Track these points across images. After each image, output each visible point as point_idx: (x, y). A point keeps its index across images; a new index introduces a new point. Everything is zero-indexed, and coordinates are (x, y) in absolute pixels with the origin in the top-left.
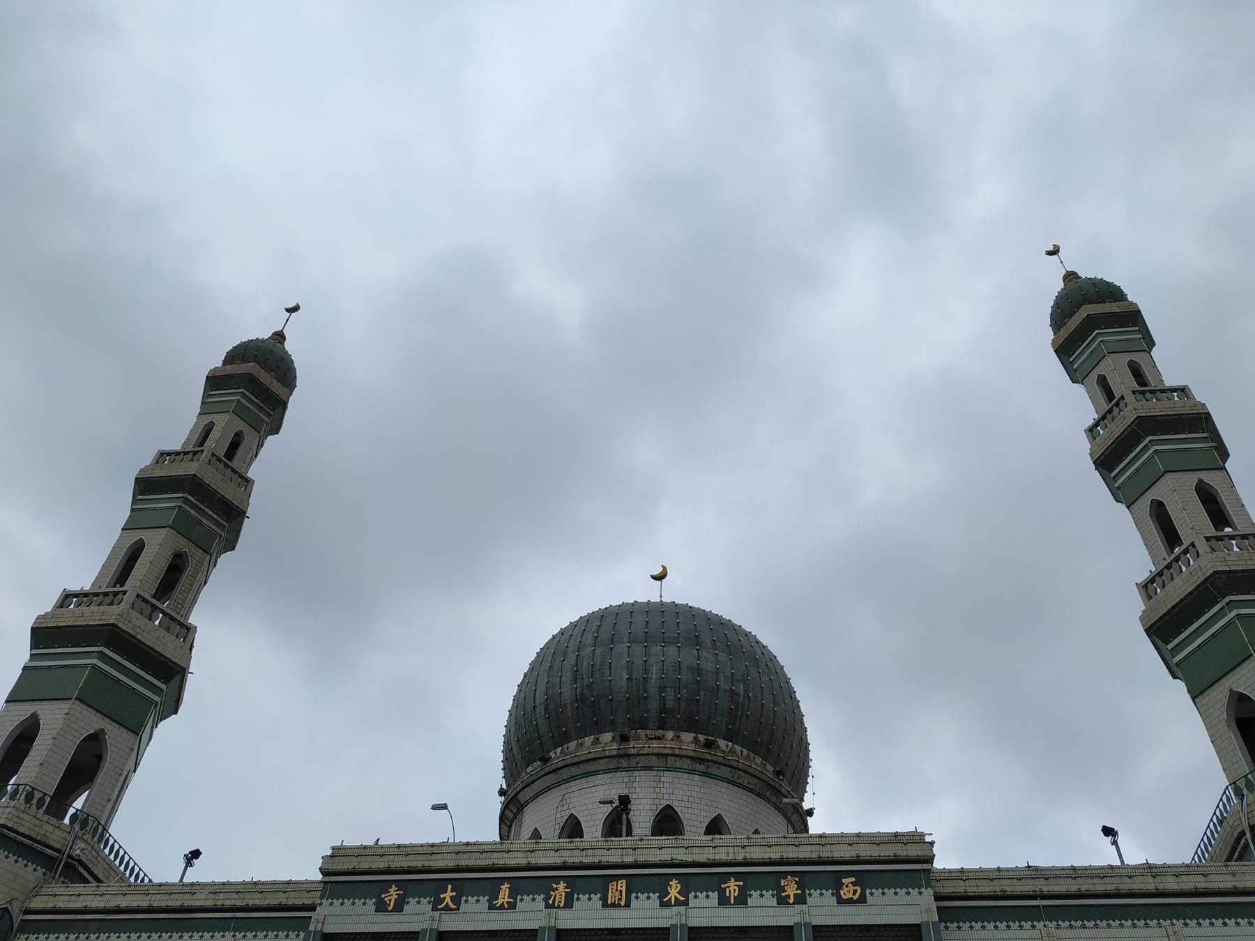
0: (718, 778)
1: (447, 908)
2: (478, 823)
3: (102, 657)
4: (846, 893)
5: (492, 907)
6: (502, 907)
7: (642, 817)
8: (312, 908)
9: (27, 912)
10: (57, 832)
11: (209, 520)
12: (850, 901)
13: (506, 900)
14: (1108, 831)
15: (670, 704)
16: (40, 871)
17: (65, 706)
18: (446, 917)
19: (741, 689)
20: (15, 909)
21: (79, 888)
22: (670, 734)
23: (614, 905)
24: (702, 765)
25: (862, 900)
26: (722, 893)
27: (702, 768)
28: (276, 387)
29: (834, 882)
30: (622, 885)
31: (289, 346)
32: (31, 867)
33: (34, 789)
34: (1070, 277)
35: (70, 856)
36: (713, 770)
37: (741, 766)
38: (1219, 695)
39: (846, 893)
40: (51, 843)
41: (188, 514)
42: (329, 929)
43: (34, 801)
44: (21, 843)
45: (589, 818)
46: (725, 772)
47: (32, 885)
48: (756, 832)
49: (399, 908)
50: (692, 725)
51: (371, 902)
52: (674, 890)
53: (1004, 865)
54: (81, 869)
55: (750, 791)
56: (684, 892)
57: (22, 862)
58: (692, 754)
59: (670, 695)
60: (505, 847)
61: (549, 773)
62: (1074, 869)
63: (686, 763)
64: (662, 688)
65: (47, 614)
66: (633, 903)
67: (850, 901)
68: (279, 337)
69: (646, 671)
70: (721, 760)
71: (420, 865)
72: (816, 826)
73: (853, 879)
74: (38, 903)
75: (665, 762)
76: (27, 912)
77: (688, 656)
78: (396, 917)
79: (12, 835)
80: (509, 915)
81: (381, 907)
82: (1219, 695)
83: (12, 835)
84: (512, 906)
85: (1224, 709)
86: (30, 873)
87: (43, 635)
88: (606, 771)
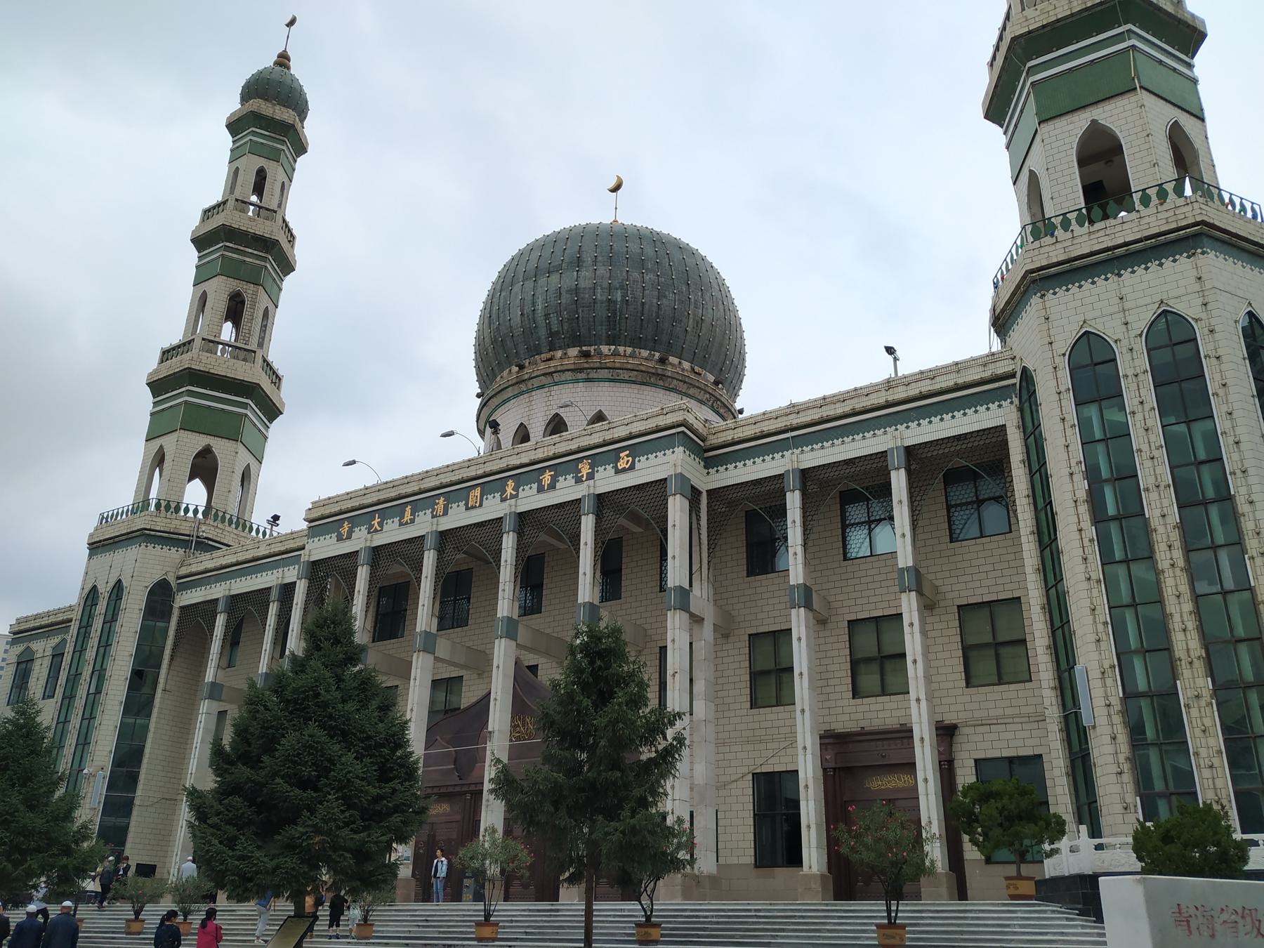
0: (600, 380)
1: (376, 531)
2: (469, 445)
3: (190, 393)
4: (621, 465)
6: (407, 523)
7: (576, 421)
8: (303, 548)
9: (179, 578)
11: (250, 257)
12: (624, 470)
14: (890, 350)
15: (555, 328)
16: (181, 551)
17: (174, 436)
18: (376, 536)
19: (618, 295)
20: (171, 579)
21: (216, 554)
22: (559, 354)
23: (473, 507)
24: (584, 373)
25: (632, 467)
26: (540, 482)
27: (583, 376)
28: (286, 115)
29: (499, 486)
30: (478, 491)
31: (296, 69)
32: (174, 550)
34: (1163, 571)
36: (593, 375)
37: (617, 365)
39: (621, 465)
41: (232, 259)
46: (604, 373)
48: (599, 417)
49: (552, 486)
50: (576, 341)
51: (334, 535)
52: (585, 469)
55: (634, 382)
56: (516, 489)
58: (572, 367)
59: (554, 319)
63: (569, 375)
64: (547, 316)
66: (485, 502)
67: (624, 470)
68: (283, 60)
69: (534, 304)
70: (598, 365)
71: (375, 499)
72: (764, 391)
74: (183, 571)
75: (552, 378)
77: (568, 280)
78: (348, 543)
80: (630, 475)
81: (340, 539)
84: (412, 521)
86: (175, 554)
87: (158, 386)
88: (515, 396)
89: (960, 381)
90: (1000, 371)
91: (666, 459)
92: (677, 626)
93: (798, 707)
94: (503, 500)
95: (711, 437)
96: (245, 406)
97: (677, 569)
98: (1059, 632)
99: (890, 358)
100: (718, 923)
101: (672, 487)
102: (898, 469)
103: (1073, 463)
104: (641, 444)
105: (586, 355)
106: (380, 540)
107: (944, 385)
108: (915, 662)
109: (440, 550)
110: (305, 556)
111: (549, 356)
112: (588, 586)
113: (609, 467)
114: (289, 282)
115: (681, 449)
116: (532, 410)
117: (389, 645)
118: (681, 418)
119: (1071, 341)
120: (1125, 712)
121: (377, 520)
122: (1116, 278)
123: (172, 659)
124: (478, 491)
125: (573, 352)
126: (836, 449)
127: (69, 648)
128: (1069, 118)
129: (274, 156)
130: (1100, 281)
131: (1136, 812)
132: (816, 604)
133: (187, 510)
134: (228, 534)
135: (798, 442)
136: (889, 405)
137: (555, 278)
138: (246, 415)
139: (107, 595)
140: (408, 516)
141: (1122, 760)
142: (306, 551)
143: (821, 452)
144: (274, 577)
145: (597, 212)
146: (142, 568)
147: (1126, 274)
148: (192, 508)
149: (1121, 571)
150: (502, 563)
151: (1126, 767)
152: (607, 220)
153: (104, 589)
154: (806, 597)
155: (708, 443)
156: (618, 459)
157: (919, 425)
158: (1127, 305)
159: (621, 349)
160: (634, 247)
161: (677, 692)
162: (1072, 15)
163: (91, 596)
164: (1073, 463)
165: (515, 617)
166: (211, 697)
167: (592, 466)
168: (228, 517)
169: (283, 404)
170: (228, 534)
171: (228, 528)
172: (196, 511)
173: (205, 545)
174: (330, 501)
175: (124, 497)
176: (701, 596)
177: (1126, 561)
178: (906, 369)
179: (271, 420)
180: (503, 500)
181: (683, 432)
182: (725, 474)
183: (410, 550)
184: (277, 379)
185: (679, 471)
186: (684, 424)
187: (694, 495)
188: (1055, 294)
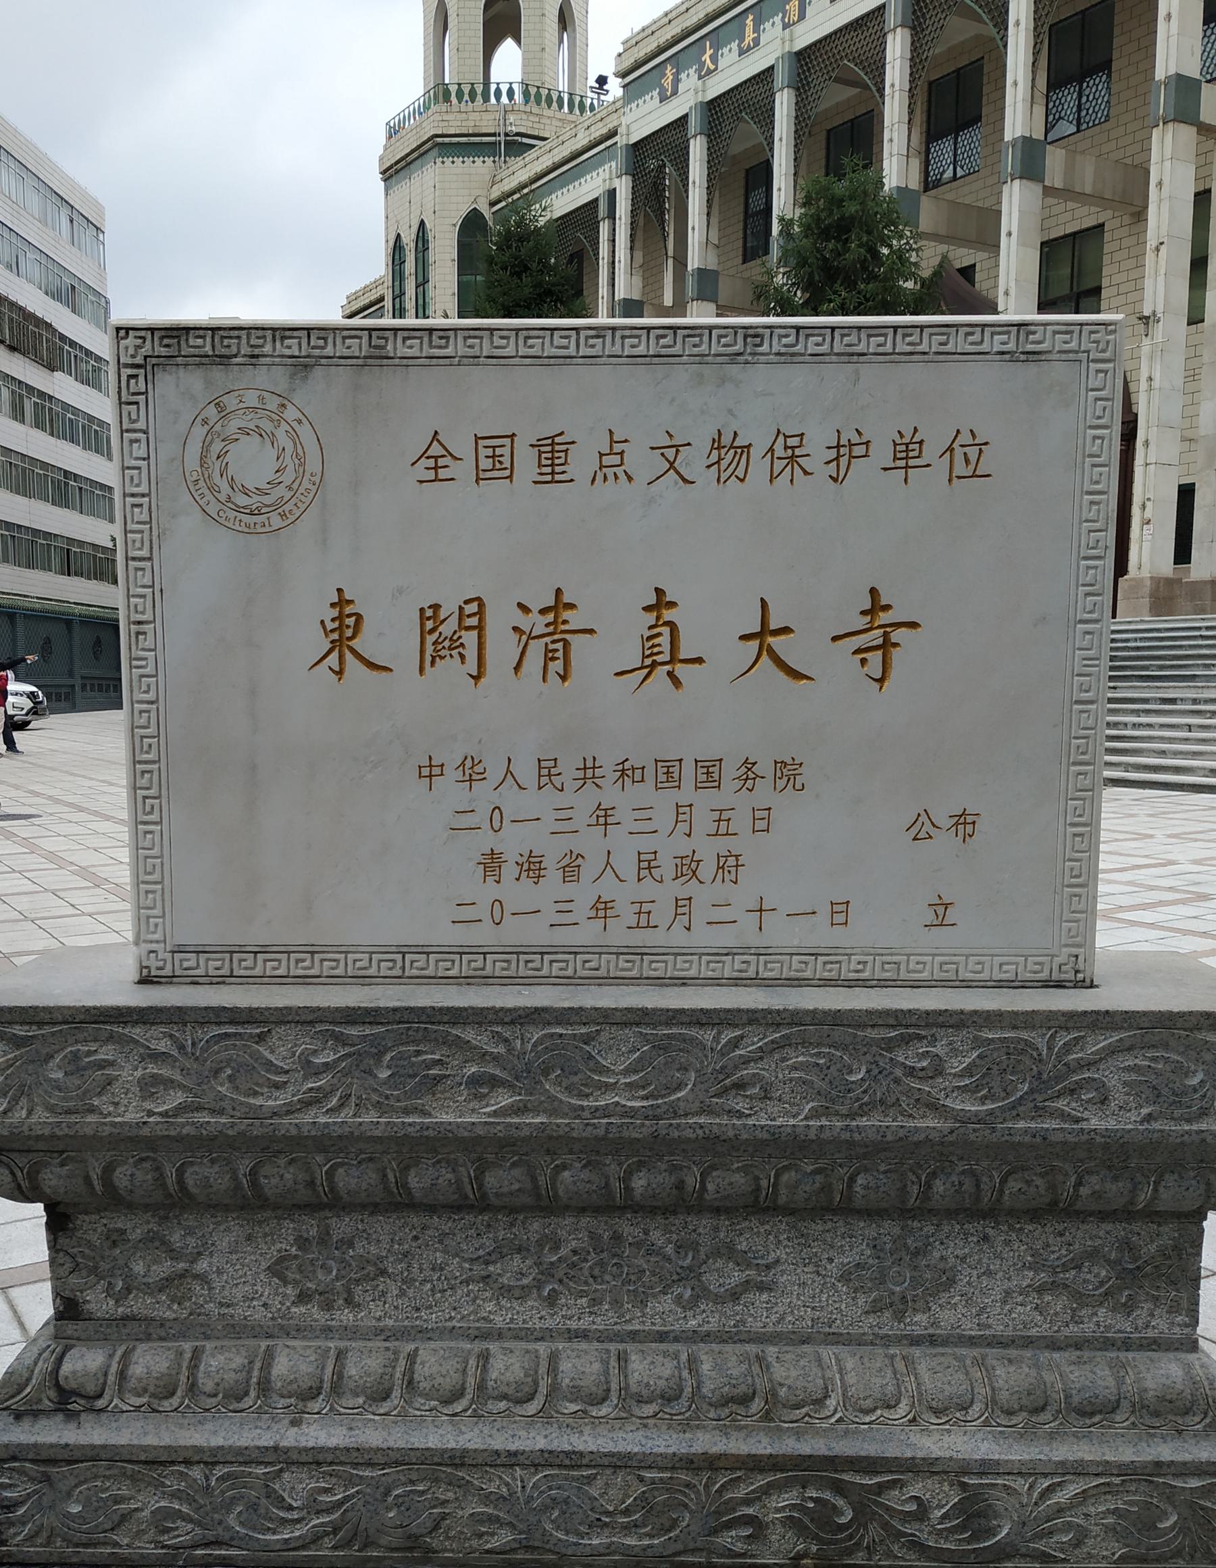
1: (709, 72)
9: (492, 204)
10: (485, 116)
13: (752, 36)
16: (489, 160)
21: (532, 154)
32: (479, 161)
33: (459, 84)
35: (506, 135)
40: (484, 131)
43: (466, 97)
44: (459, 143)
47: (488, 178)
56: (714, 59)
57: (468, 160)
71: (701, 15)
73: (748, 1531)
74: (495, 193)
76: (492, 204)
78: (675, 102)
79: (447, 140)
83: (447, 140)
84: (757, 42)
86: (481, 167)
92: (1168, 153)
97: (1174, 41)
98: (398, 300)
100: (1138, 649)
106: (718, 86)
109: (801, 87)
112: (1020, 106)
121: (709, 52)
127: (64, 387)
133: (498, 93)
134: (547, 122)
139: (413, 245)
140: (750, 35)
144: (600, 179)
146: (453, 192)
148: (504, 88)
150: (888, 90)
153: (408, 239)
161: (1161, 279)
163: (397, 248)
168: (544, 92)
170: (547, 122)
171: (547, 112)
172: (511, 93)
173: (516, 146)
174: (648, 32)
175: (409, 86)
183: (751, 98)
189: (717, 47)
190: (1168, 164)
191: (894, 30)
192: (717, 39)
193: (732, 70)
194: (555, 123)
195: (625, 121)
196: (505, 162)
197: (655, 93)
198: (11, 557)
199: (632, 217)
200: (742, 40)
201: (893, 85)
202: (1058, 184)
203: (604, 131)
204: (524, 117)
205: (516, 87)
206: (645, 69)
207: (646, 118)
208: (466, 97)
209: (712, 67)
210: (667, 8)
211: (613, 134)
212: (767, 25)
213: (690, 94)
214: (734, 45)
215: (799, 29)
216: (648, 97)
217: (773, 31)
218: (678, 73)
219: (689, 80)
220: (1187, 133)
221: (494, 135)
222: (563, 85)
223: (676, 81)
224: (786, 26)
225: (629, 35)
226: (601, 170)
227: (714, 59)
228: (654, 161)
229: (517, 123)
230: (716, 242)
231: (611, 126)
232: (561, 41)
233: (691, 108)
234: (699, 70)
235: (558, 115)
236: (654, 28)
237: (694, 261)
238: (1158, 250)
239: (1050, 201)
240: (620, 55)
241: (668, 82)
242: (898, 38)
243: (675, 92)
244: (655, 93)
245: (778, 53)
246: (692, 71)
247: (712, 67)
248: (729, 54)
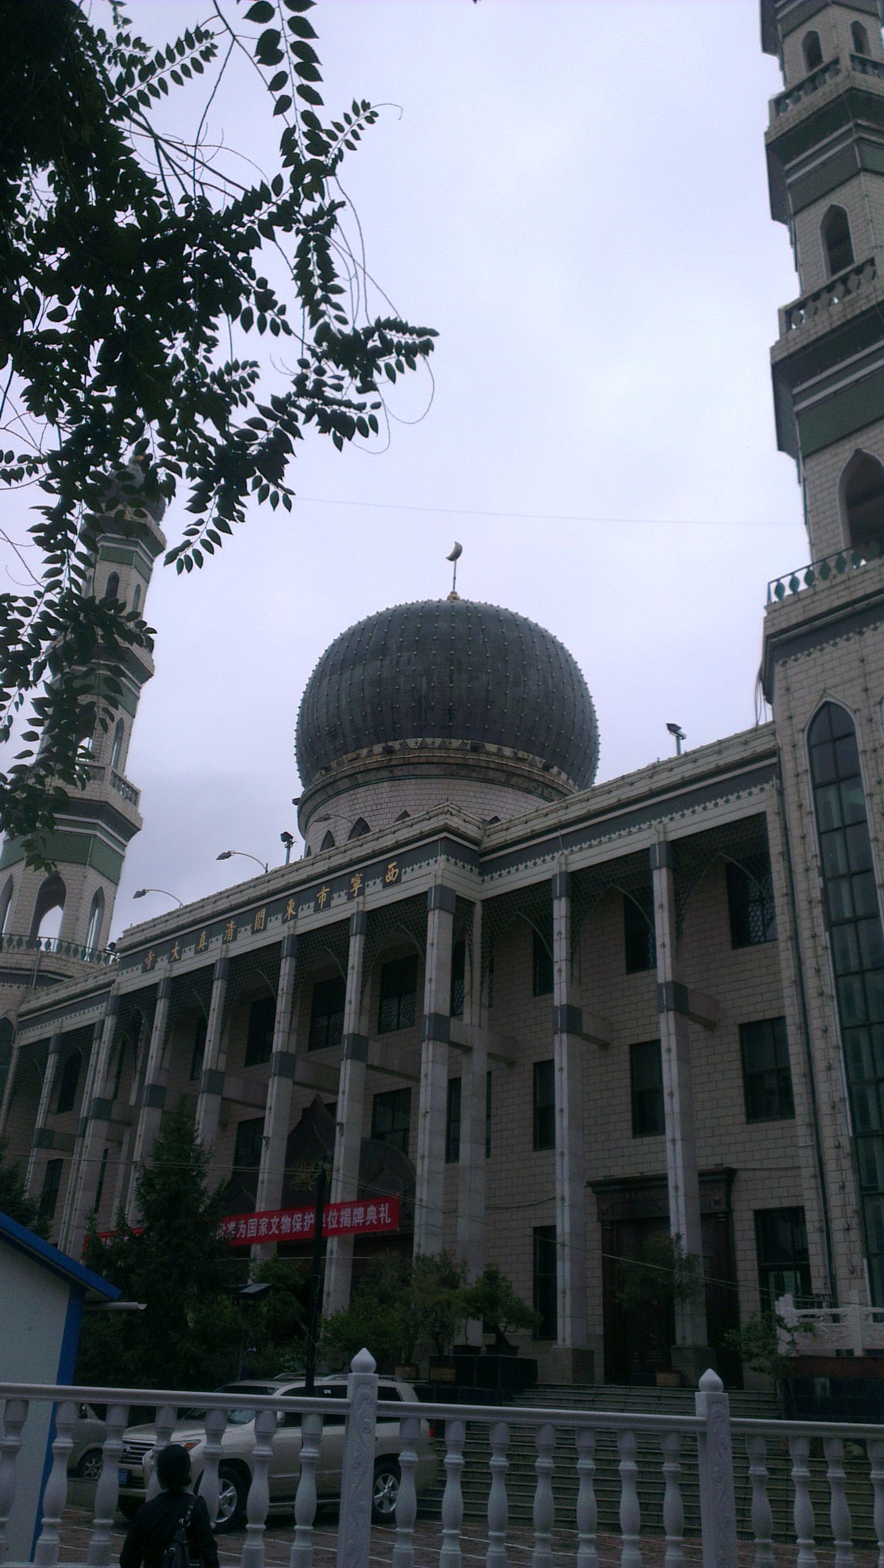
1: (175, 960)
4: (390, 878)
5: (254, 932)
9: (20, 1016)
14: (673, 728)
16: (23, 987)
20: (12, 1017)
22: (365, 752)
23: (259, 931)
24: (392, 770)
25: (398, 881)
30: (262, 913)
32: (15, 987)
33: (11, 935)
38: (840, 457)
39: (390, 878)
42: (123, 991)
43: (15, 943)
45: (373, 818)
49: (327, 905)
52: (357, 885)
53: (704, 744)
54: (50, 975)
56: (296, 909)
60: (58, 956)
61: (345, 777)
62: (720, 742)
65: (777, 343)
66: (269, 925)
67: (391, 883)
71: (174, 925)
73: (395, 863)
74: (24, 1008)
82: (840, 457)
85: (836, 489)
86: (15, 991)
89: (721, 763)
90: (760, 749)
91: (423, 871)
93: (558, 1150)
94: (284, 921)
95: (486, 839)
96: (94, 826)
99: (673, 738)
101: (432, 901)
102: (660, 868)
103: (809, 855)
104: (409, 854)
105: (389, 751)
106: (237, 949)
107: (705, 768)
108: (671, 1094)
110: (113, 991)
111: (354, 755)
113: (378, 881)
114: (148, 690)
115: (444, 857)
116: (342, 812)
117: (321, 1055)
118: (441, 823)
119: (811, 714)
120: (855, 1155)
121: (177, 948)
122: (857, 637)
123: (11, 1102)
124: (262, 913)
125: (378, 748)
126: (604, 848)
128: (831, 451)
129: (125, 559)
130: (842, 642)
131: (863, 1278)
132: (588, 1025)
135: (569, 841)
136: (652, 794)
137: (358, 671)
138: (95, 836)
141: (850, 1214)
142: (115, 985)
143: (592, 852)
145: (430, 588)
147: (868, 632)
149: (856, 983)
150: (555, 937)
151: (854, 1222)
152: (438, 593)
154: (572, 1021)
155: (483, 846)
156: (386, 870)
157: (683, 816)
158: (870, 668)
159: (429, 741)
160: (443, 625)
162: (833, 331)
164: (809, 855)
165: (292, 1051)
166: (39, 1145)
167: (363, 880)
169: (141, 820)
171: (73, 960)
173: (46, 979)
174: (140, 928)
176: (471, 1023)
177: (862, 972)
178: (687, 746)
179: (128, 837)
180: (284, 921)
181: (445, 837)
182: (499, 882)
184: (133, 795)
185: (439, 882)
186: (446, 828)
187: (461, 909)
188: (796, 660)
189: (183, 946)
190: (430, 1064)
191: (286, 957)
192: (184, 941)
193: (190, 961)
194: (77, 966)
195: (118, 980)
196: (35, 989)
197: (140, 966)
198: (702, 1179)
199: (114, 1043)
200: (198, 944)
201: (283, 990)
202: (376, 1064)
203: (106, 981)
204: (55, 961)
205: (52, 941)
206: (144, 946)
207: (133, 980)
208: (15, 943)
209: (178, 957)
210: (154, 917)
211: (109, 984)
212: (214, 939)
213: (162, 971)
214: (193, 947)
215: (232, 945)
216: (135, 968)
217: (216, 944)
218: (156, 957)
219: (162, 963)
220: (443, 1048)
221: (30, 970)
222: (90, 943)
223: (154, 962)
224: (224, 942)
225: (129, 927)
226: (100, 1006)
227: (180, 953)
228: (133, 1010)
229: (48, 965)
230: (167, 1068)
231: (112, 978)
232: (93, 915)
233: (284, 938)
234: (169, 958)
235: (80, 962)
236: (144, 927)
237: (149, 1079)
238: (425, 1116)
239: (370, 1071)
240: (120, 939)
241: (149, 961)
242: (288, 962)
243: (153, 968)
244: (140, 966)
245: (218, 957)
246: (165, 957)
247: (178, 957)
248: (189, 952)
